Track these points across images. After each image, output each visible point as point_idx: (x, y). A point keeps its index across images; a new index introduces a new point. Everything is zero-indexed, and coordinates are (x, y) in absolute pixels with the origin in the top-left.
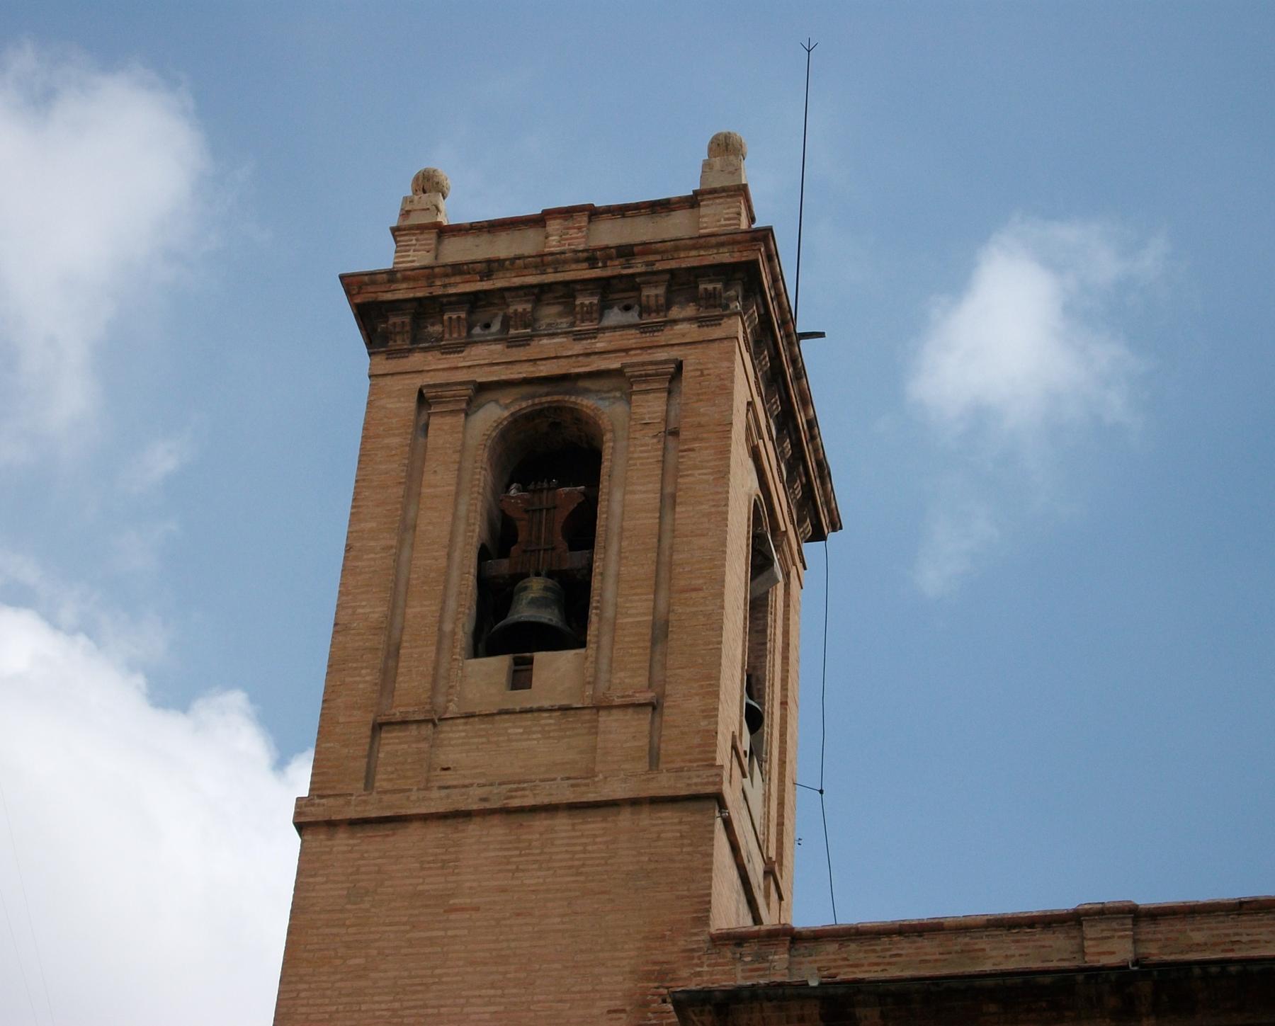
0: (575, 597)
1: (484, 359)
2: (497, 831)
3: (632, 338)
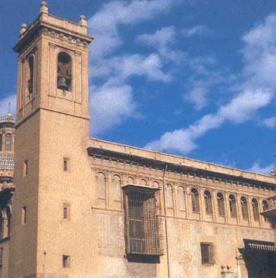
0: (69, 82)
1: (56, 41)
2: (65, 116)
3: (75, 46)
